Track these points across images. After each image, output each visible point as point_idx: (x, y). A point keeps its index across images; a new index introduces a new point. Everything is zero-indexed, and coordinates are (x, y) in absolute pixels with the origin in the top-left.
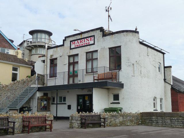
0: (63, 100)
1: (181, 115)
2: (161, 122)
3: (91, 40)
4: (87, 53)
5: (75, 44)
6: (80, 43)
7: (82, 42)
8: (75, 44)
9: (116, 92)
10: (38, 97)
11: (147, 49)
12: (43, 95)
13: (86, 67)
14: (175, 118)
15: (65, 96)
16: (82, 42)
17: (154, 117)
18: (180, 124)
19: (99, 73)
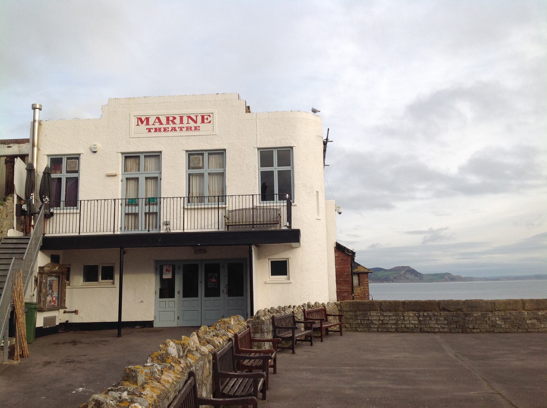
0: (229, 285)
1: (446, 308)
2: (394, 322)
3: (203, 121)
4: (191, 154)
5: (148, 124)
6: (168, 123)
7: (174, 123)
8: (148, 124)
9: (280, 257)
10: (41, 268)
11: (127, 184)
12: (50, 262)
13: (138, 189)
14: (431, 313)
15: (114, 264)
16: (174, 123)
17: (373, 313)
18: (443, 326)
19: (231, 204)
